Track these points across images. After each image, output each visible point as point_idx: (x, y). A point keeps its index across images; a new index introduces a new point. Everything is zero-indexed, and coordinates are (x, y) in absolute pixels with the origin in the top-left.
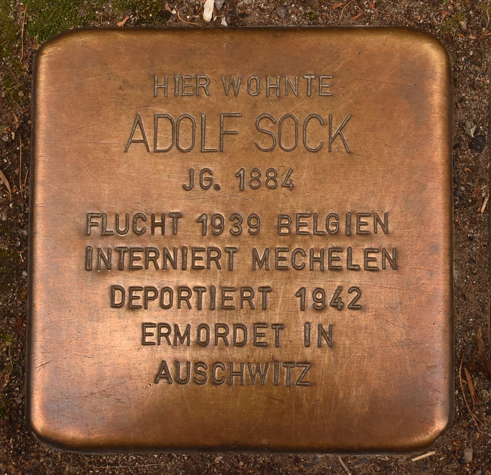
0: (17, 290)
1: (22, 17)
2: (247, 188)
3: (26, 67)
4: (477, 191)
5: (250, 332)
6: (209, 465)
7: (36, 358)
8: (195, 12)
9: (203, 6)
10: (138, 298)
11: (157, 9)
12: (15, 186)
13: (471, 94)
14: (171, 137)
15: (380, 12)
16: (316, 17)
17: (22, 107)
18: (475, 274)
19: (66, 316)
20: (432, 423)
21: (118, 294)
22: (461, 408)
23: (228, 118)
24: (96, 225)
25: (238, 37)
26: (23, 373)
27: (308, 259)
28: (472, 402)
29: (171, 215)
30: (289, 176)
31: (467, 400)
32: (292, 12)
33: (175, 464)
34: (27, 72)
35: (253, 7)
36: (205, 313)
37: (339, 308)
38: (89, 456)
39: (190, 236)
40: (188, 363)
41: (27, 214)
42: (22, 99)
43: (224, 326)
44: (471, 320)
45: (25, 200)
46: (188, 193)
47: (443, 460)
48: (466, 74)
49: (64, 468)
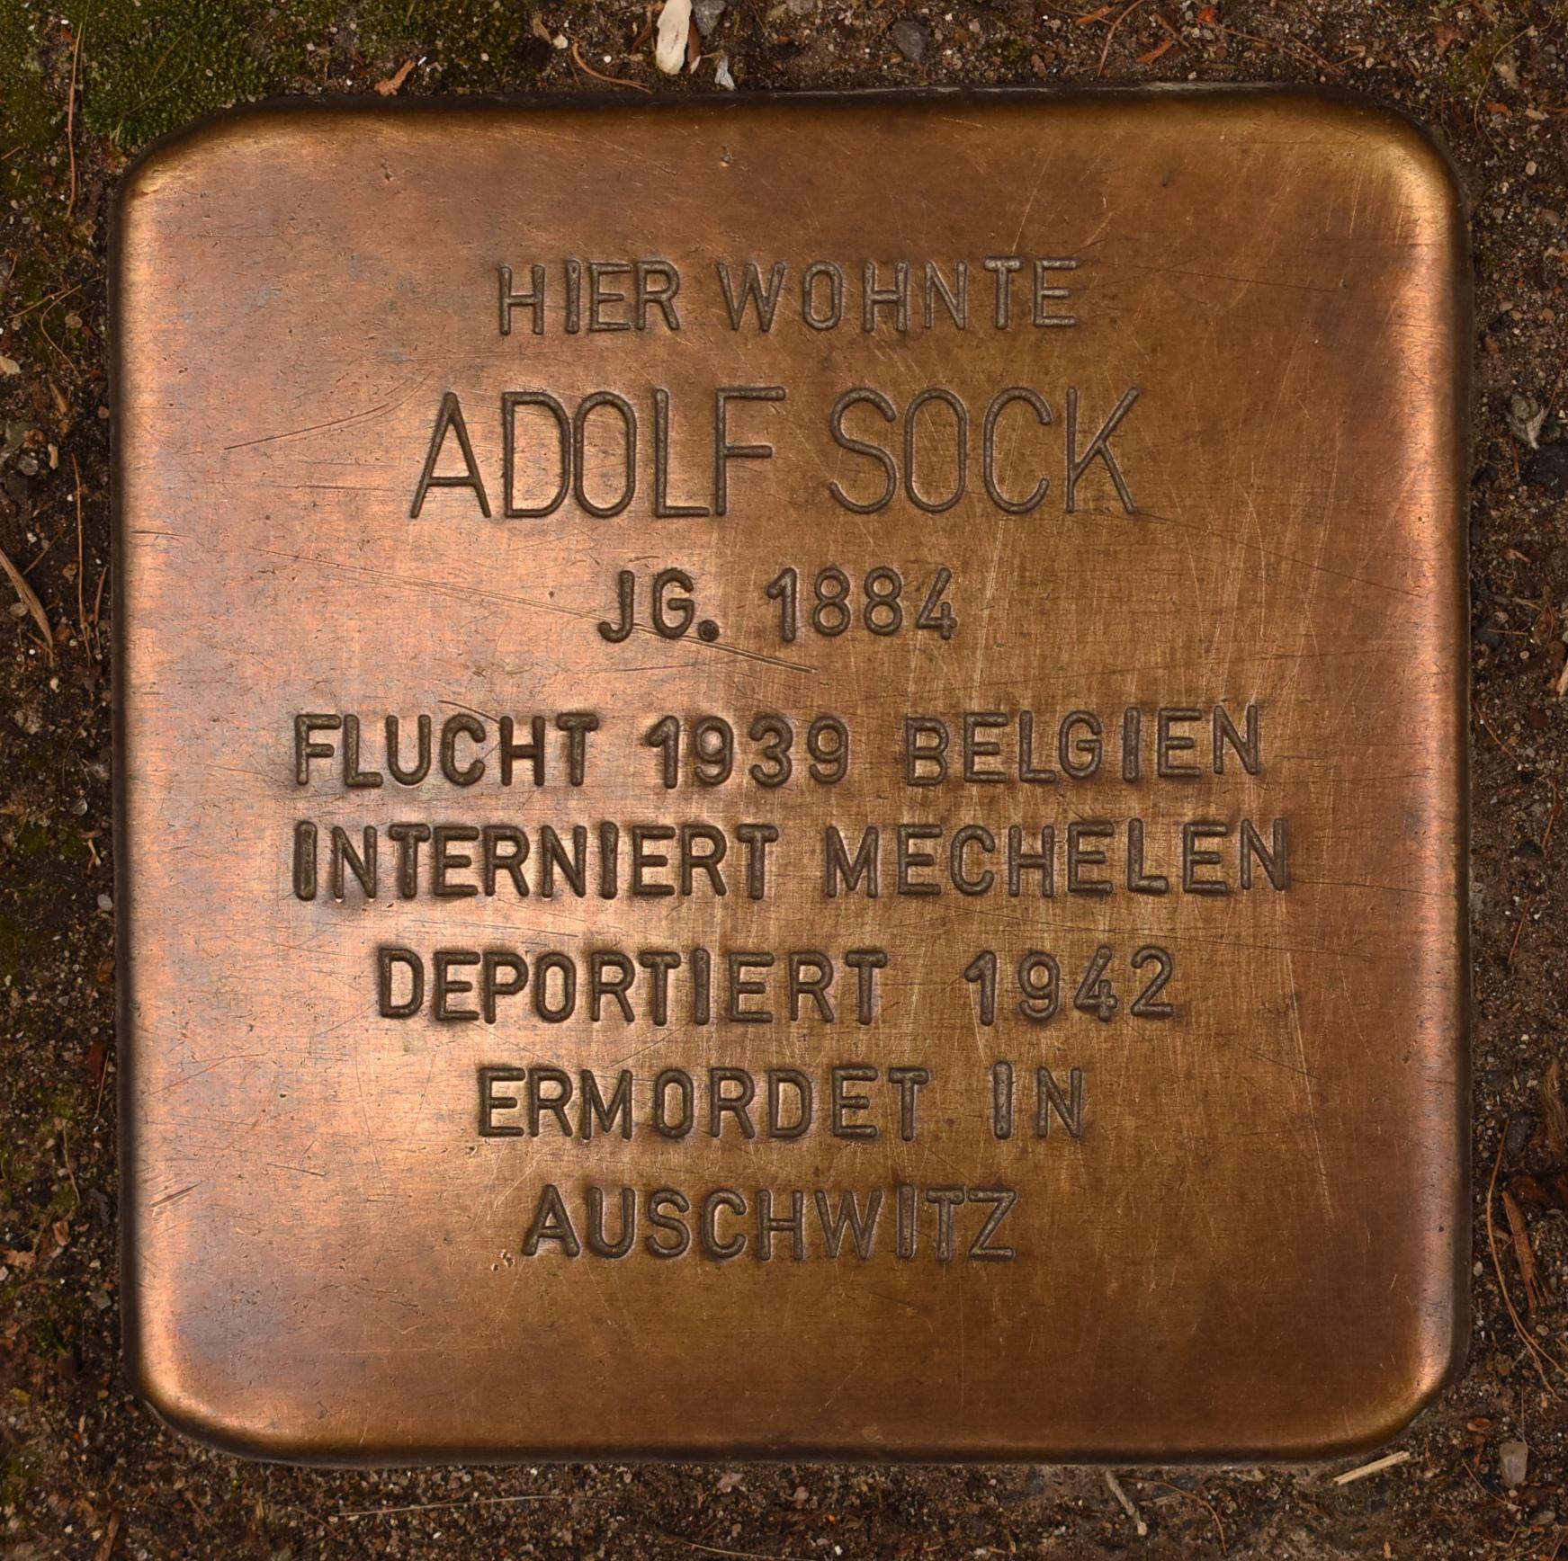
0: (83, 953)
1: (67, 66)
2: (803, 630)
3: (86, 230)
4: (1548, 625)
5: (822, 1092)
6: (700, 1499)
7: (149, 1176)
8: (630, 43)
9: (654, 22)
10: (464, 987)
11: (505, 37)
12: (64, 620)
13: (1530, 305)
14: (557, 469)
15: (1232, 37)
16: (1025, 56)
17: (77, 362)
18: (1540, 890)
19: (238, 1044)
20: (1402, 1360)
21: (401, 973)
22: (1492, 1316)
23: (741, 403)
24: (326, 751)
25: (771, 134)
26: (112, 1216)
27: (1004, 858)
28: (1526, 1300)
29: (563, 721)
30: (940, 592)
31: (1509, 1291)
32: (946, 39)
33: (596, 1494)
34: (89, 248)
35: (818, 21)
36: (679, 1035)
37: (1104, 1012)
38: (326, 1474)
39: (624, 781)
40: (626, 1192)
41: (106, 710)
42: (78, 337)
43: (739, 1075)
44: (1525, 1037)
45: (99, 669)
46: (615, 648)
47: (1435, 1476)
48: (1516, 238)
49: (250, 1510)
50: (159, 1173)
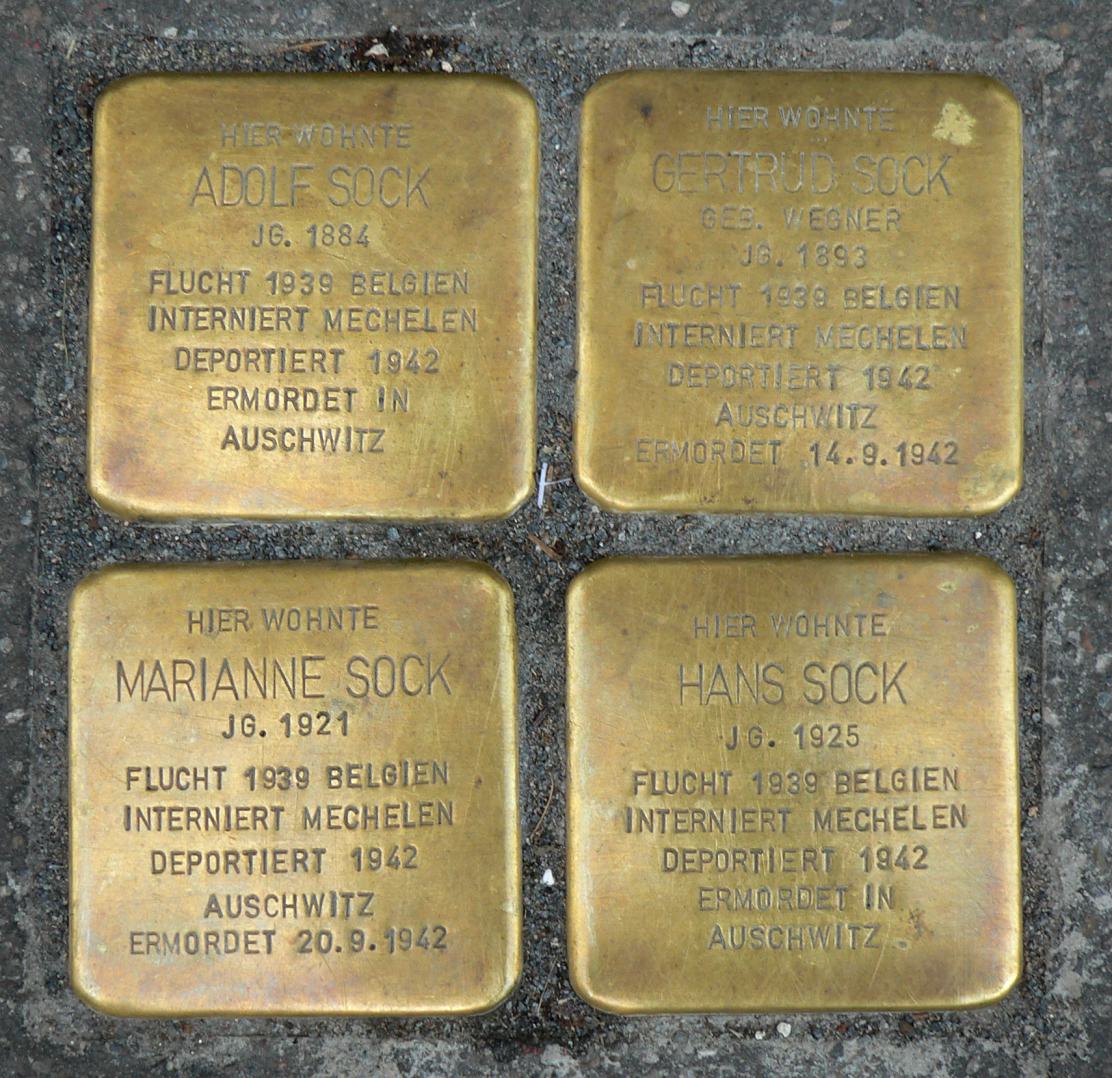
50: (82, 918)
